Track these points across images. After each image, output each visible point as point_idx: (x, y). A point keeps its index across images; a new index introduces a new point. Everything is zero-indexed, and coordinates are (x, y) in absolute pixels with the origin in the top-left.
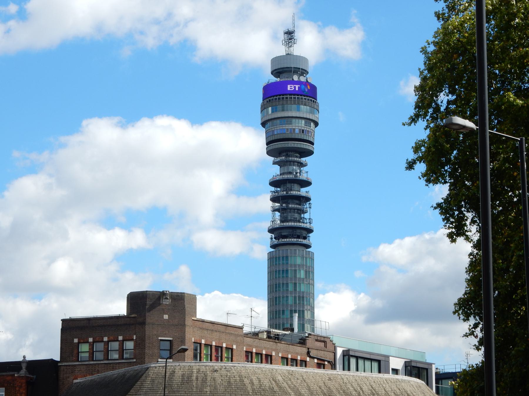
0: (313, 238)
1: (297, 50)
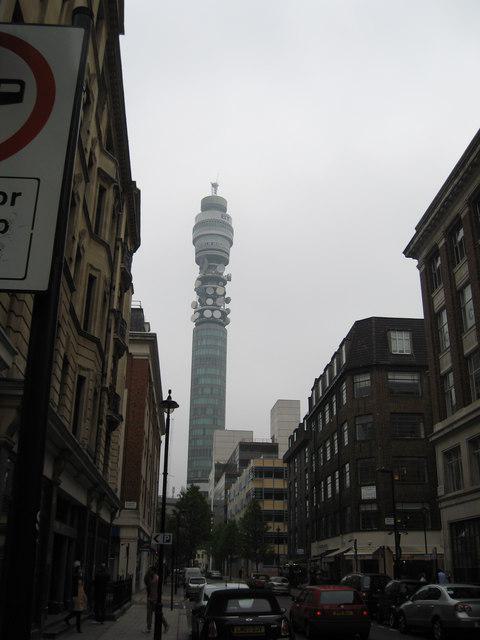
1: (219, 194)
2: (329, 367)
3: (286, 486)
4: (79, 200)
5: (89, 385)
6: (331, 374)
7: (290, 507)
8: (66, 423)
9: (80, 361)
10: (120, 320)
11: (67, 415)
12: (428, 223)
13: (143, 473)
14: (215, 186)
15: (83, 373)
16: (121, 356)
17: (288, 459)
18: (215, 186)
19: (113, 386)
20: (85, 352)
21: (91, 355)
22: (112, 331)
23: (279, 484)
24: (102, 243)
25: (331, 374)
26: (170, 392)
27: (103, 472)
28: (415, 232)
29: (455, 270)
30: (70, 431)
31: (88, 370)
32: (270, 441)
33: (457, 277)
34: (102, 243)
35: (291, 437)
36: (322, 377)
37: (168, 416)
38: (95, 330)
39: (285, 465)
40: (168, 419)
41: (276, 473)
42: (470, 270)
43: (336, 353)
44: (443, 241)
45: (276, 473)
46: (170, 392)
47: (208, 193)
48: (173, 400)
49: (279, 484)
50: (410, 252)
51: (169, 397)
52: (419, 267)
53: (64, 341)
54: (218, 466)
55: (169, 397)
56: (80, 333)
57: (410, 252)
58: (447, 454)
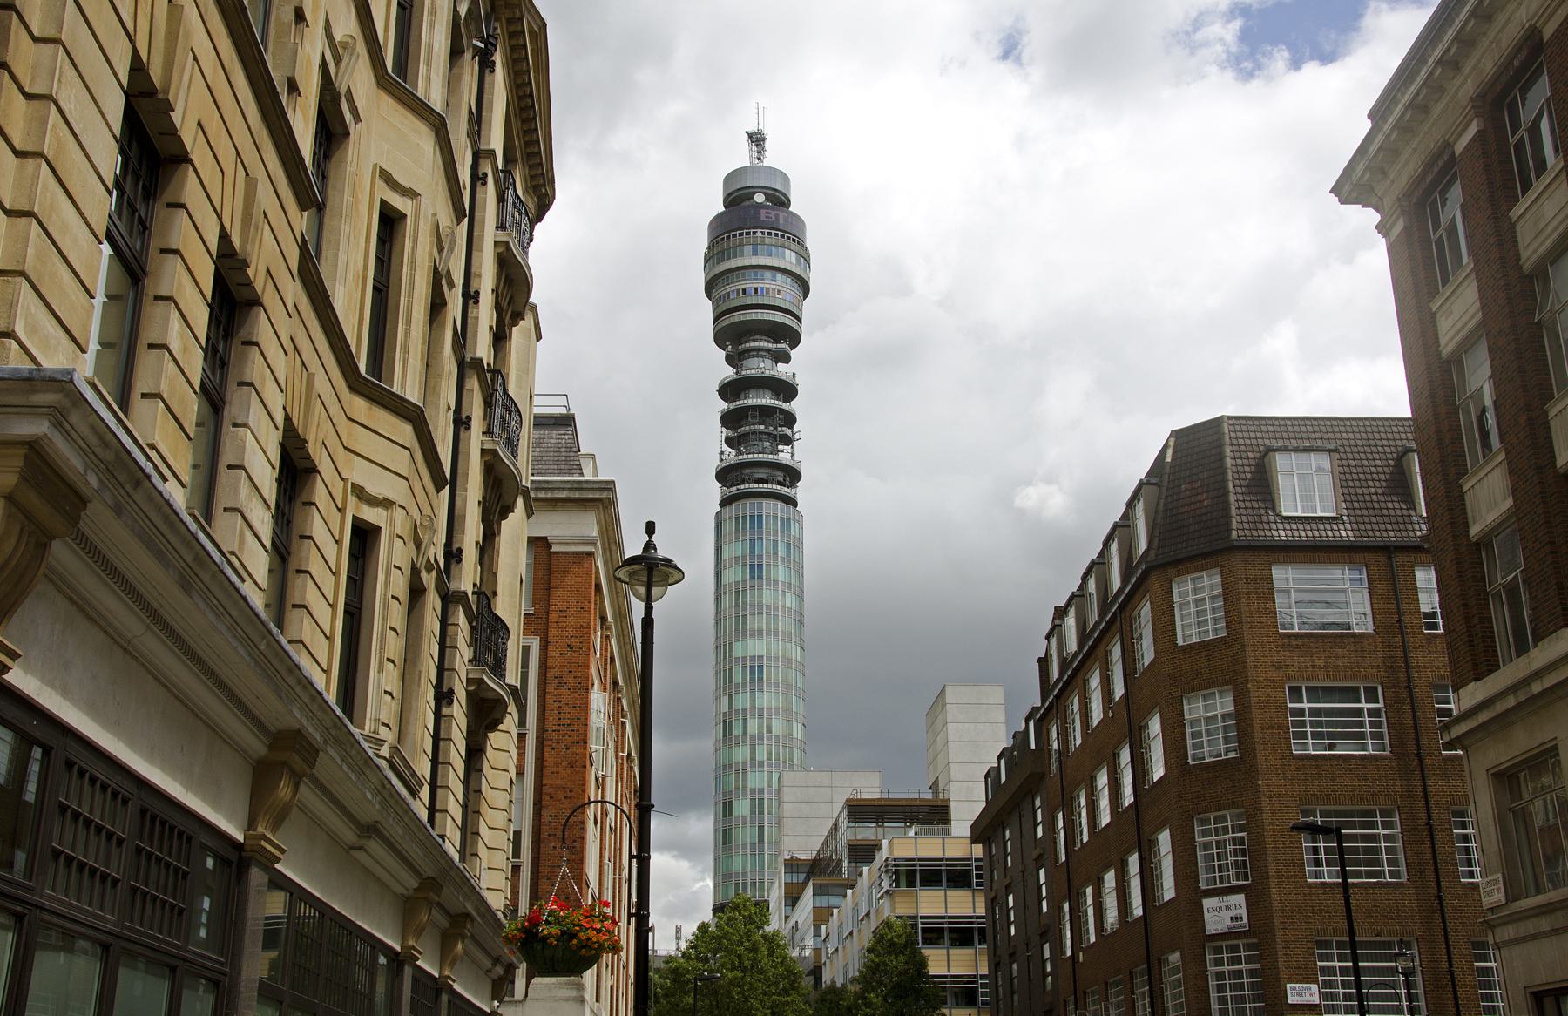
0: (801, 492)
1: (769, 161)
2: (1098, 566)
3: (981, 911)
4: (451, 285)
5: (392, 556)
6: (1104, 585)
7: (995, 965)
8: (319, 680)
9: (359, 473)
10: (499, 396)
11: (321, 648)
12: (1419, 81)
13: (592, 871)
14: (757, 139)
15: (371, 515)
16: (507, 510)
17: (984, 831)
18: (757, 139)
19: (486, 595)
20: (363, 441)
21: (400, 460)
22: (477, 426)
23: (962, 904)
24: (420, 109)
25: (1104, 585)
26: (650, 528)
27: (462, 852)
28: (1368, 125)
29: (1515, 213)
30: (332, 698)
31: (386, 503)
32: (928, 795)
33: (1524, 234)
34: (420, 109)
35: (992, 774)
36: (1077, 598)
37: (649, 610)
38: (407, 382)
39: (978, 850)
40: (648, 622)
41: (956, 876)
42: (1481, 297)
43: (1115, 527)
44: (1473, 129)
45: (956, 876)
46: (650, 528)
47: (742, 157)
48: (661, 552)
49: (962, 904)
50: (1350, 188)
51: (649, 546)
52: (1382, 228)
53: (280, 363)
54: (792, 865)
55: (649, 546)
56: (356, 384)
57: (1350, 188)
58: (1506, 779)
